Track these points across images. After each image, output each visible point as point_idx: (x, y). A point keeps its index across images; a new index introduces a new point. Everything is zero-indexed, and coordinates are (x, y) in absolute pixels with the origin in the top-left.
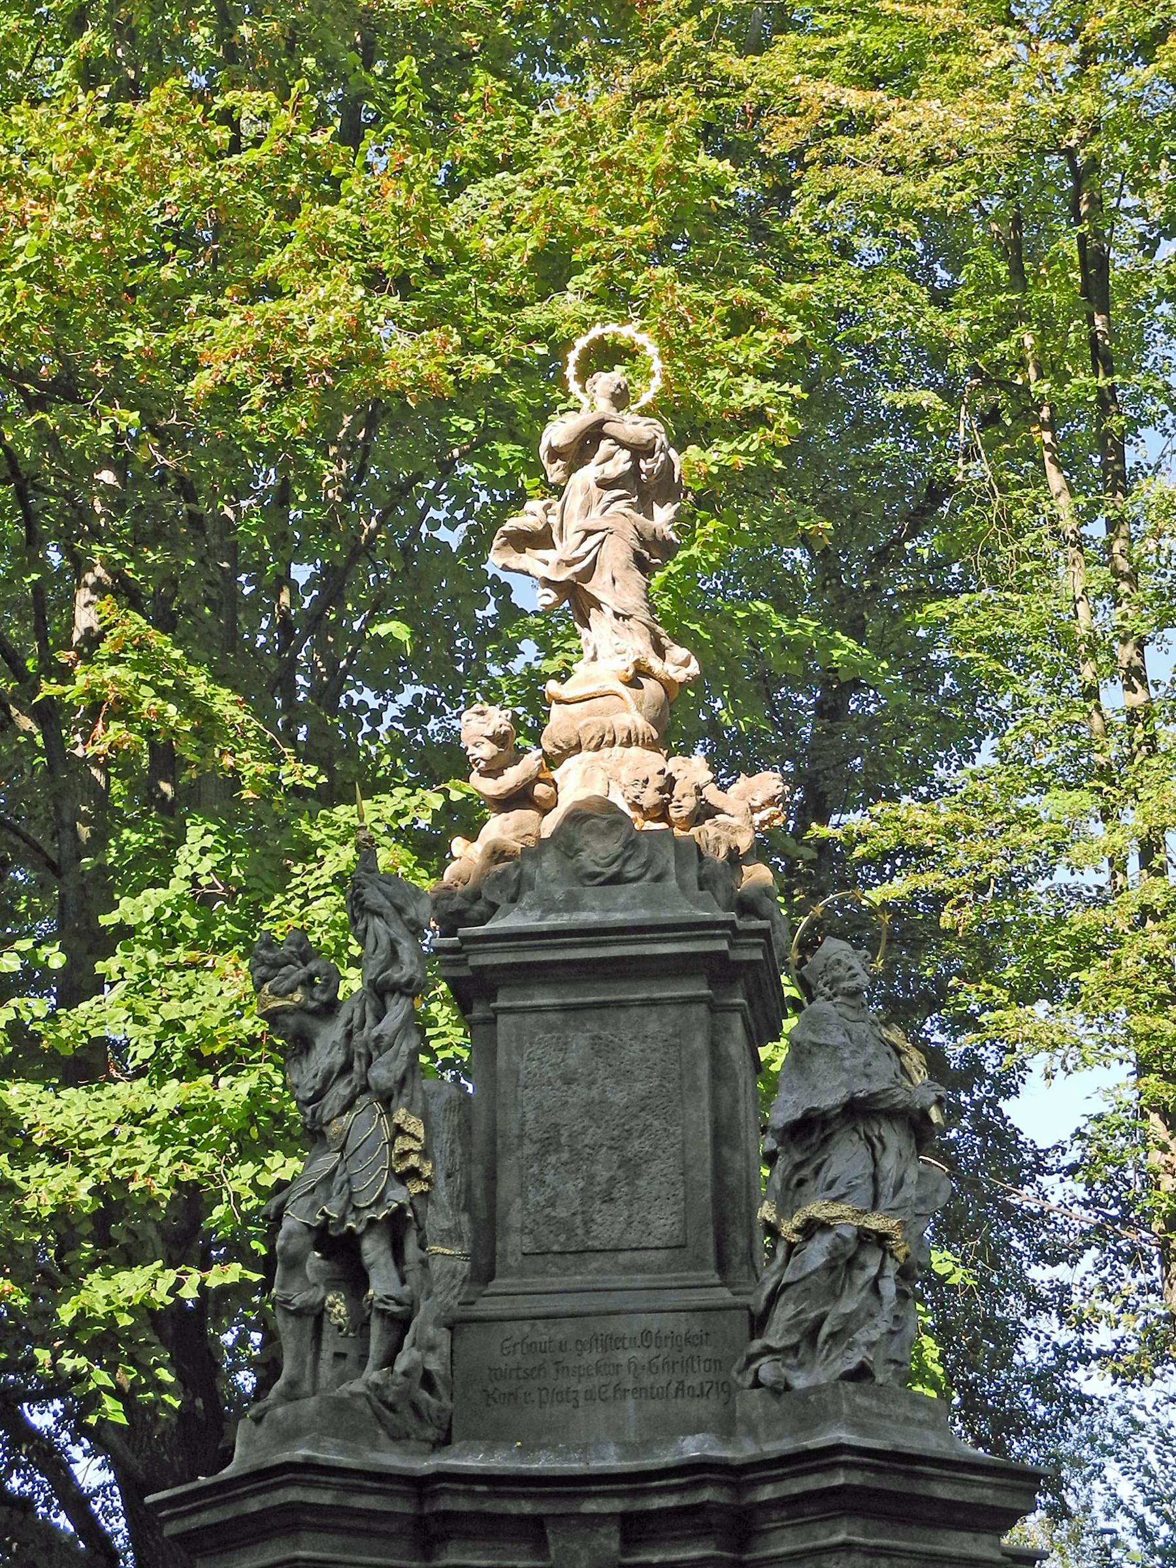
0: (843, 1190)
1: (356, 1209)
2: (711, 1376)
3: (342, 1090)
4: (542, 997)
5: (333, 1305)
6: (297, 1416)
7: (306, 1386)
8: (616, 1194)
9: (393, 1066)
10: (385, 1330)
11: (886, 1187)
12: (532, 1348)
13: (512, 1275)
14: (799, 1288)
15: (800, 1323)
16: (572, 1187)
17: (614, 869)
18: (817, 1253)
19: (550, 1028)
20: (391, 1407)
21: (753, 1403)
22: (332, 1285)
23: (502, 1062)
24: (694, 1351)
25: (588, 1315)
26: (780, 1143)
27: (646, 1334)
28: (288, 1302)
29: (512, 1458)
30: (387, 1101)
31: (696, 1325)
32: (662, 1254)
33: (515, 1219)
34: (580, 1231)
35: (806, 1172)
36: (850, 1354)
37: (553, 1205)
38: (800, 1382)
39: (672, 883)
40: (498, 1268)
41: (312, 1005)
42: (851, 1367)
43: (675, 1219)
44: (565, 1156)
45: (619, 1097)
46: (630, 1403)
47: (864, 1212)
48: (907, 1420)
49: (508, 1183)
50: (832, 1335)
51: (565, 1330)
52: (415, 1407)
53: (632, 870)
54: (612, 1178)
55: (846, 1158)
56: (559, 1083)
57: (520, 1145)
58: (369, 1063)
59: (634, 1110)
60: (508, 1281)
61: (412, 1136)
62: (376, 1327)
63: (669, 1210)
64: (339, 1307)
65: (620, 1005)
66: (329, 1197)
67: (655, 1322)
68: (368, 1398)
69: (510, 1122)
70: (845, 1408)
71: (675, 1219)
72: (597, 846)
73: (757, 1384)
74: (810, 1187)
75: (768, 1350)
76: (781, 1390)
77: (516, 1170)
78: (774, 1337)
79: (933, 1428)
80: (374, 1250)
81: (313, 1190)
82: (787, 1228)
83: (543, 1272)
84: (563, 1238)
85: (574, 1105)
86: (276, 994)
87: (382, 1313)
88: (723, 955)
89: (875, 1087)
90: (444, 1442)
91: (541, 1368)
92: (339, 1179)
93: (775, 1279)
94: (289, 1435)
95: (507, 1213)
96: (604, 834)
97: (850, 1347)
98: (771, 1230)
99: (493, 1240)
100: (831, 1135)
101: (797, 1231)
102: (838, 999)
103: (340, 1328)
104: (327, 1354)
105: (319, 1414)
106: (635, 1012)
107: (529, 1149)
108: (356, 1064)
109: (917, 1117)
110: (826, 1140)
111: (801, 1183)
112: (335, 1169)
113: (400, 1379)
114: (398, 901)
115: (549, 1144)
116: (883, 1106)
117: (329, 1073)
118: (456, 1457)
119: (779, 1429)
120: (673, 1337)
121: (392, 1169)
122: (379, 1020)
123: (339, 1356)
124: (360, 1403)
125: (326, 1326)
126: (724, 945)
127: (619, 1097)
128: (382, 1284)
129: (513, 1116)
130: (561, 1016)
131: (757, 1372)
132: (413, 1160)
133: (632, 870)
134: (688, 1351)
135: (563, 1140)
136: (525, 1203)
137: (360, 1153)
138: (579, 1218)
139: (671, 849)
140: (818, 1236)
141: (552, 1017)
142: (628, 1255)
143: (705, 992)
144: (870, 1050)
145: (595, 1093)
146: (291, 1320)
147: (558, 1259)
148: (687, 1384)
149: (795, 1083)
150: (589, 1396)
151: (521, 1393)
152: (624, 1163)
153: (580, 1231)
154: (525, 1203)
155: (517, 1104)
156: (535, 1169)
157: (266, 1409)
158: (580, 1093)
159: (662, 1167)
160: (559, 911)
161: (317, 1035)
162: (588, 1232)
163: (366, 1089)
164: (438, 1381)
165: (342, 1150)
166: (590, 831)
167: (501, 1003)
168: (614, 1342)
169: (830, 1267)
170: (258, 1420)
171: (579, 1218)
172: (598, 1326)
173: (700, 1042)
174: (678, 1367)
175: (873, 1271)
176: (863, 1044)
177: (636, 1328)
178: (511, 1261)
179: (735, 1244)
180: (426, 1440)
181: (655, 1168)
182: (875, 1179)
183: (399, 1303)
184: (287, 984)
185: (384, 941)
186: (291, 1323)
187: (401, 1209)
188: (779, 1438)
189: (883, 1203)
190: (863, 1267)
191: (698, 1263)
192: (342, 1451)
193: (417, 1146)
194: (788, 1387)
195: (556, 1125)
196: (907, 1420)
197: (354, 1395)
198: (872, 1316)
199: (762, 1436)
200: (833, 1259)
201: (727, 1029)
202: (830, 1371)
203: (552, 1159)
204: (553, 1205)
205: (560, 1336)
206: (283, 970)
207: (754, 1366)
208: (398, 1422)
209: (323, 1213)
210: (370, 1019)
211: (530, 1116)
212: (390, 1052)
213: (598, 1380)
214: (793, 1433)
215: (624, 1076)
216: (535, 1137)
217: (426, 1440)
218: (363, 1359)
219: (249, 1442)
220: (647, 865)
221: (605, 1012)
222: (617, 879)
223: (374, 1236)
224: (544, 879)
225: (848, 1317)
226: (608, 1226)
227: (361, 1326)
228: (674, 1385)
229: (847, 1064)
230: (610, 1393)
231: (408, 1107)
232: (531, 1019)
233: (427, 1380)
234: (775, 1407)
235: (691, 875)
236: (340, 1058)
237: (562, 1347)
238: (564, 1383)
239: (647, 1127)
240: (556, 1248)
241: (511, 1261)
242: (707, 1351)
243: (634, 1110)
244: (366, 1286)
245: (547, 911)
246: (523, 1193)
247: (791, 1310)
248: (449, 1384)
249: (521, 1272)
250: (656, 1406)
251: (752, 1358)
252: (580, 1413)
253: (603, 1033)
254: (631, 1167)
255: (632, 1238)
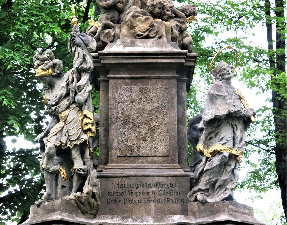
0: (226, 141)
1: (70, 141)
2: (178, 197)
3: (66, 102)
4: (124, 74)
5: (61, 171)
6: (53, 206)
7: (53, 196)
8: (147, 139)
9: (84, 95)
10: (79, 179)
11: (237, 141)
12: (122, 186)
13: (114, 163)
14: (211, 171)
15: (210, 182)
16: (133, 136)
17: (146, 34)
18: (216, 161)
19: (126, 84)
20: (83, 204)
21: (195, 206)
22: (61, 164)
23: (111, 94)
24: (173, 189)
25: (140, 176)
26: (205, 126)
27: (158, 183)
28: (49, 169)
29: (120, 220)
30: (81, 107)
31: (169, 181)
32: (162, 158)
33: (115, 145)
34: (136, 150)
35: (213, 135)
36: (226, 192)
37: (127, 141)
38: (209, 200)
39: (165, 39)
40: (109, 160)
41: (54, 74)
42: (227, 196)
43: (165, 147)
44: (131, 126)
45: (148, 108)
46: (153, 204)
47: (231, 149)
48: (243, 213)
49: (113, 134)
50: (220, 186)
51: (133, 180)
52: (89, 204)
53: (152, 34)
54: (146, 133)
55: (226, 133)
56: (129, 102)
57: (117, 122)
58: (75, 95)
59: (153, 112)
60: (111, 165)
61: (90, 118)
62: (75, 178)
63: (164, 144)
64: (63, 172)
65: (149, 78)
66: (61, 137)
67: (161, 180)
68: (76, 201)
69: (113, 114)
70: (226, 209)
71: (165, 147)
72: (141, 26)
73: (196, 200)
74: (214, 139)
75: (200, 190)
76: (204, 203)
77: (115, 130)
78: (202, 185)
79: (249, 215)
80: (75, 154)
81: (56, 134)
82: (207, 153)
83: (124, 162)
84: (130, 152)
85: (134, 110)
86: (43, 70)
87: (79, 174)
88: (182, 64)
89: (236, 109)
90: (95, 216)
91: (124, 192)
92: (65, 131)
93: (202, 168)
94: (52, 211)
95: (112, 143)
96: (143, 22)
97: (226, 190)
98: (202, 153)
99: (108, 151)
100: (221, 124)
101: (211, 153)
102: (224, 81)
103: (63, 178)
104: (59, 186)
105: (61, 205)
106: (154, 81)
107: (119, 123)
108: (71, 94)
109: (246, 119)
110: (219, 126)
111: (211, 138)
112: (63, 128)
113: (86, 195)
114: (87, 42)
115: (126, 122)
116: (238, 115)
117: (61, 96)
118: (102, 219)
119: (203, 214)
120: (166, 184)
121: (82, 129)
122: (78, 81)
123: (63, 187)
124: (73, 202)
125: (59, 177)
126: (183, 61)
127: (148, 108)
128: (78, 165)
129: (114, 112)
130: (130, 81)
131: (196, 196)
132: (90, 126)
133: (152, 34)
134: (171, 189)
135: (130, 120)
136: (118, 140)
137: (72, 123)
138: (136, 145)
139: (164, 28)
140: (217, 155)
141: (127, 81)
142: (151, 158)
143: (176, 75)
144: (234, 97)
145: (141, 106)
146: (49, 175)
147: (129, 159)
148: (171, 199)
149: (210, 106)
150: (140, 202)
151: (118, 200)
152: (150, 129)
153: (136, 150)
154: (118, 140)
155: (116, 108)
156: (122, 130)
157: (41, 203)
158: (136, 106)
159: (163, 130)
160: (129, 46)
161: (56, 84)
162: (138, 150)
163: (74, 102)
164: (97, 196)
165: (65, 121)
166: (138, 21)
167: (110, 76)
168: (148, 185)
169: (220, 165)
170: (38, 206)
171: (136, 145)
172: (142, 180)
173: (174, 91)
174: (168, 194)
175: (233, 167)
176: (232, 96)
177: (154, 181)
178: (113, 158)
179: (183, 155)
180: (92, 214)
181: (160, 130)
182: (234, 138)
183: (84, 171)
184: (47, 67)
185: (81, 55)
186: (49, 176)
187: (85, 141)
188: (204, 217)
189: (237, 146)
190: (230, 165)
191: (173, 162)
192: (69, 216)
193: (91, 122)
194: (206, 202)
195: (128, 116)
196: (243, 213)
197: (71, 199)
198: (232, 180)
199: (198, 216)
200: (222, 163)
201: (182, 87)
202: (220, 197)
203: (127, 127)
204: (127, 141)
205: (130, 183)
206: (46, 62)
207: (196, 195)
208: (85, 208)
209: (60, 142)
210: (75, 80)
211: (120, 112)
212: (83, 91)
213: (142, 197)
214: (208, 216)
215: (150, 101)
216: (121, 119)
217: (92, 214)
218: (71, 188)
219: (35, 213)
220: (157, 33)
221: (144, 80)
222: (147, 37)
223: (76, 149)
224: (123, 35)
225: (225, 181)
226: (145, 148)
227: (70, 178)
228: (166, 199)
229: (228, 102)
230: (146, 201)
231: (88, 109)
232: (120, 81)
233: (94, 196)
234: (202, 207)
235: (170, 37)
236: (65, 92)
237: (131, 186)
238: (131, 198)
239: (157, 117)
240: (128, 155)
241: (113, 158)
242: (177, 189)
243: (153, 112)
244: (72, 164)
245: (126, 46)
246: (117, 137)
247: (207, 178)
248: (100, 197)
249: (116, 162)
250: (160, 205)
251: (194, 192)
252: (137, 207)
253: (144, 87)
254: (152, 130)
255: (152, 153)
